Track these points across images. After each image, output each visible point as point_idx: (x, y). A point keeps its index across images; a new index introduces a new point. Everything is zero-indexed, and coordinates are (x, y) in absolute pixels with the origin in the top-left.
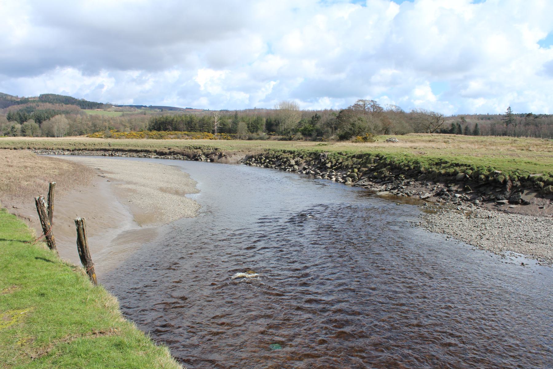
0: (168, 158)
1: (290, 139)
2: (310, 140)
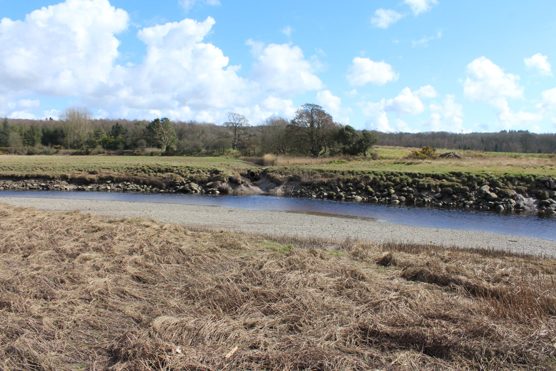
0: (106, 190)
1: (87, 153)
2: (114, 154)
